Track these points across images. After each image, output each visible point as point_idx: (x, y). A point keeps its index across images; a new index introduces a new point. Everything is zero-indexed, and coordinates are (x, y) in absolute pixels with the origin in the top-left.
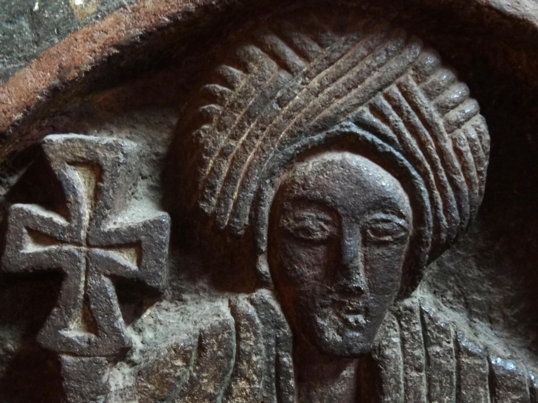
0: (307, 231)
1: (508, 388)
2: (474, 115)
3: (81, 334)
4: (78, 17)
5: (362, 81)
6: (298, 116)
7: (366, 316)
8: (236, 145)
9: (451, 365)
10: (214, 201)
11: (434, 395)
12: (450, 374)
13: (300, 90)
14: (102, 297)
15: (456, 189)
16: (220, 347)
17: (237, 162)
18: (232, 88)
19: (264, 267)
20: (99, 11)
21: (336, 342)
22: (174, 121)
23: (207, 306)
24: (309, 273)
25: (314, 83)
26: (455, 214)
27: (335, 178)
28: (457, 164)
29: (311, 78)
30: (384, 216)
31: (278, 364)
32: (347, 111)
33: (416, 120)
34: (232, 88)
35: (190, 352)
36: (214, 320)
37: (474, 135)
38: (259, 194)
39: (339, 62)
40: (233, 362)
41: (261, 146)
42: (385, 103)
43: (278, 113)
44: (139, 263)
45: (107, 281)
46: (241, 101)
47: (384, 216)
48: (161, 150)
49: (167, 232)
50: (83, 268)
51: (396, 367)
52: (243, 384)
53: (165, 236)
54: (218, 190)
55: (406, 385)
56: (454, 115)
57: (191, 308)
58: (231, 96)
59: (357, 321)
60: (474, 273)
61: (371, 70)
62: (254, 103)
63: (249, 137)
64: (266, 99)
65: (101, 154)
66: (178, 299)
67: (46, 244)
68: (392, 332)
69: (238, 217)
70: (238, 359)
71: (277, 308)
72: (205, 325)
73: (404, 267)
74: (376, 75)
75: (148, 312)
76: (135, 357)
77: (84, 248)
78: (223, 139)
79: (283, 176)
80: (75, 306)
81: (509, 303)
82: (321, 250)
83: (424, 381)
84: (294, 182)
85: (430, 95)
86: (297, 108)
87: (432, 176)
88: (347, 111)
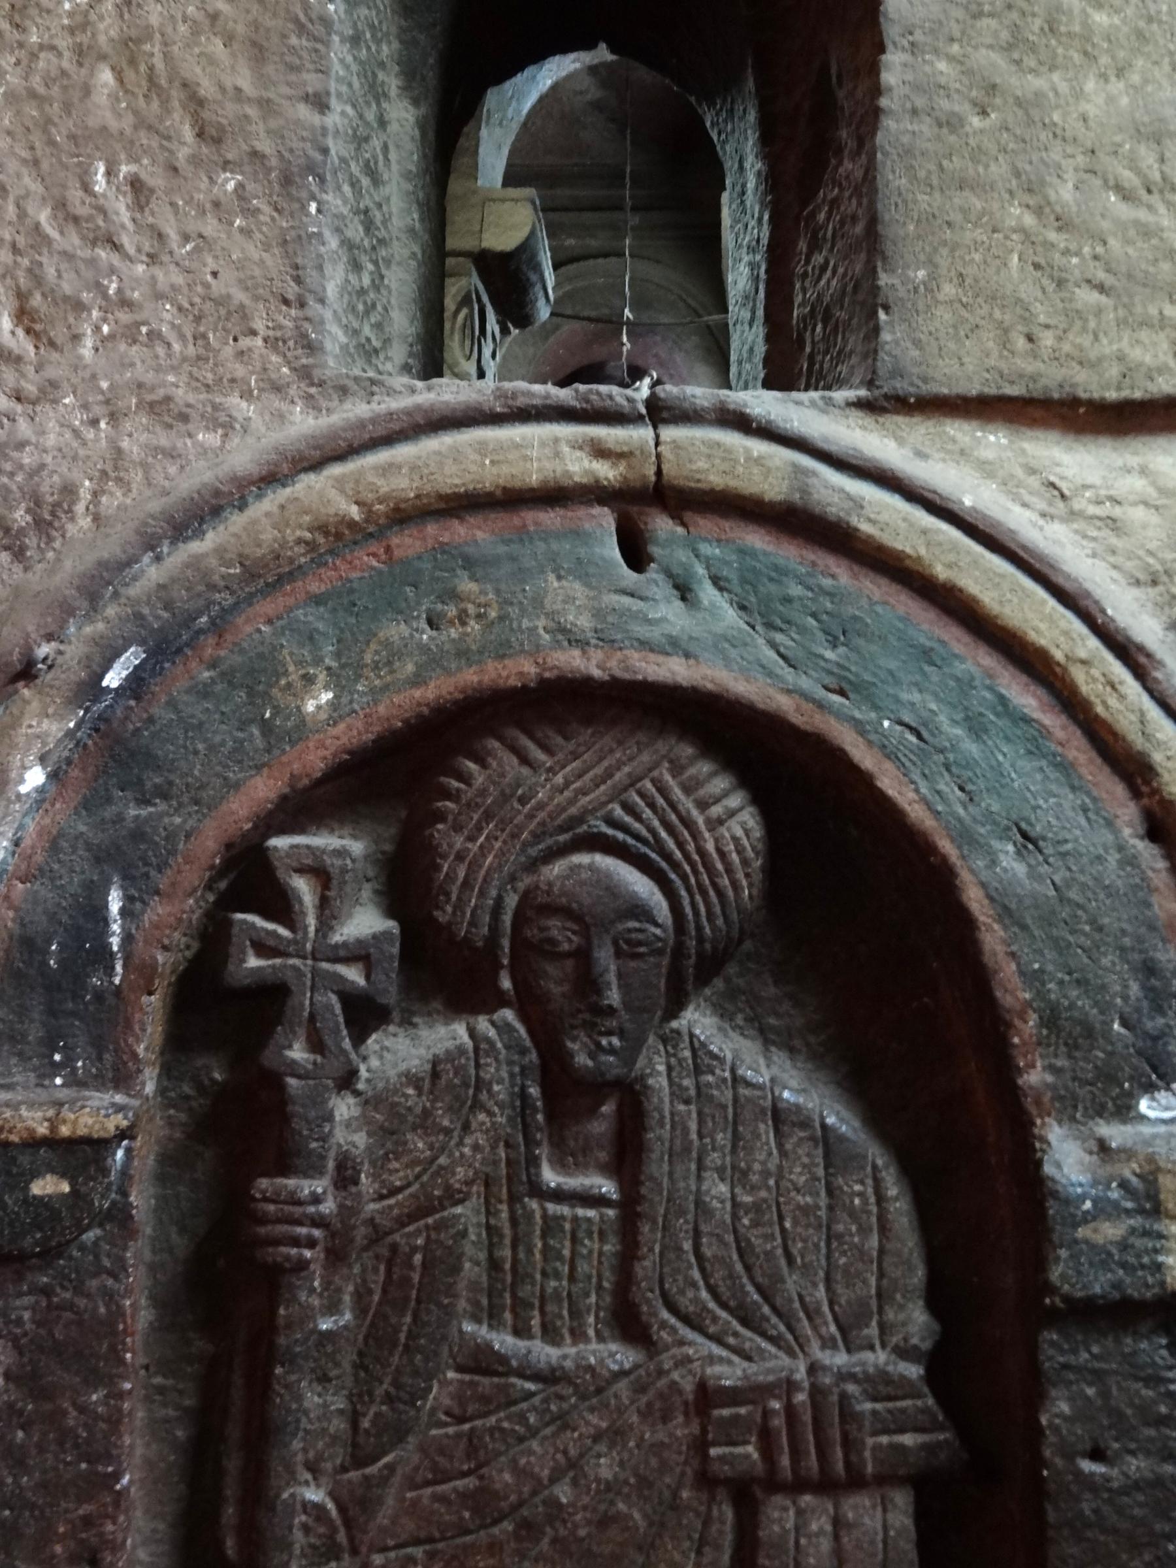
0: (552, 942)
1: (794, 1124)
2: (741, 809)
3: (306, 1056)
4: (310, 724)
5: (611, 776)
6: (542, 815)
7: (621, 1039)
8: (474, 847)
10: (449, 909)
11: (705, 1131)
12: (724, 1107)
13: (543, 787)
14: (328, 1016)
15: (720, 894)
16: (456, 1074)
18: (469, 784)
19: (506, 984)
20: (331, 717)
21: (586, 1066)
22: (403, 814)
23: (442, 1031)
24: (556, 990)
25: (559, 779)
26: (720, 922)
27: (582, 883)
28: (719, 866)
29: (555, 774)
30: (637, 925)
31: (523, 1095)
32: (595, 810)
34: (469, 784)
35: (423, 1079)
36: (450, 1044)
37: (739, 833)
38: (499, 901)
39: (585, 756)
40: (471, 1092)
41: (500, 849)
42: (638, 799)
43: (519, 812)
44: (368, 977)
45: (334, 999)
46: (478, 800)
47: (637, 925)
48: (388, 847)
49: (398, 944)
50: (309, 983)
51: (661, 1100)
52: (482, 1117)
53: (396, 950)
54: (454, 897)
55: (672, 1120)
56: (716, 810)
57: (424, 1033)
58: (469, 794)
59: (610, 1044)
60: (771, 991)
62: (493, 802)
63: (487, 838)
64: (505, 798)
66: (407, 1022)
67: (268, 957)
68: (656, 1058)
69: (476, 927)
70: (478, 1089)
71: (522, 1031)
72: (439, 1049)
73: (668, 981)
74: (627, 769)
75: (374, 1036)
76: (361, 1086)
77: (309, 962)
78: (459, 841)
79: (526, 882)
80: (300, 1024)
82: (569, 964)
83: (694, 1115)
84: (537, 887)
85: (687, 790)
86: (541, 806)
87: (693, 880)
88: (595, 810)
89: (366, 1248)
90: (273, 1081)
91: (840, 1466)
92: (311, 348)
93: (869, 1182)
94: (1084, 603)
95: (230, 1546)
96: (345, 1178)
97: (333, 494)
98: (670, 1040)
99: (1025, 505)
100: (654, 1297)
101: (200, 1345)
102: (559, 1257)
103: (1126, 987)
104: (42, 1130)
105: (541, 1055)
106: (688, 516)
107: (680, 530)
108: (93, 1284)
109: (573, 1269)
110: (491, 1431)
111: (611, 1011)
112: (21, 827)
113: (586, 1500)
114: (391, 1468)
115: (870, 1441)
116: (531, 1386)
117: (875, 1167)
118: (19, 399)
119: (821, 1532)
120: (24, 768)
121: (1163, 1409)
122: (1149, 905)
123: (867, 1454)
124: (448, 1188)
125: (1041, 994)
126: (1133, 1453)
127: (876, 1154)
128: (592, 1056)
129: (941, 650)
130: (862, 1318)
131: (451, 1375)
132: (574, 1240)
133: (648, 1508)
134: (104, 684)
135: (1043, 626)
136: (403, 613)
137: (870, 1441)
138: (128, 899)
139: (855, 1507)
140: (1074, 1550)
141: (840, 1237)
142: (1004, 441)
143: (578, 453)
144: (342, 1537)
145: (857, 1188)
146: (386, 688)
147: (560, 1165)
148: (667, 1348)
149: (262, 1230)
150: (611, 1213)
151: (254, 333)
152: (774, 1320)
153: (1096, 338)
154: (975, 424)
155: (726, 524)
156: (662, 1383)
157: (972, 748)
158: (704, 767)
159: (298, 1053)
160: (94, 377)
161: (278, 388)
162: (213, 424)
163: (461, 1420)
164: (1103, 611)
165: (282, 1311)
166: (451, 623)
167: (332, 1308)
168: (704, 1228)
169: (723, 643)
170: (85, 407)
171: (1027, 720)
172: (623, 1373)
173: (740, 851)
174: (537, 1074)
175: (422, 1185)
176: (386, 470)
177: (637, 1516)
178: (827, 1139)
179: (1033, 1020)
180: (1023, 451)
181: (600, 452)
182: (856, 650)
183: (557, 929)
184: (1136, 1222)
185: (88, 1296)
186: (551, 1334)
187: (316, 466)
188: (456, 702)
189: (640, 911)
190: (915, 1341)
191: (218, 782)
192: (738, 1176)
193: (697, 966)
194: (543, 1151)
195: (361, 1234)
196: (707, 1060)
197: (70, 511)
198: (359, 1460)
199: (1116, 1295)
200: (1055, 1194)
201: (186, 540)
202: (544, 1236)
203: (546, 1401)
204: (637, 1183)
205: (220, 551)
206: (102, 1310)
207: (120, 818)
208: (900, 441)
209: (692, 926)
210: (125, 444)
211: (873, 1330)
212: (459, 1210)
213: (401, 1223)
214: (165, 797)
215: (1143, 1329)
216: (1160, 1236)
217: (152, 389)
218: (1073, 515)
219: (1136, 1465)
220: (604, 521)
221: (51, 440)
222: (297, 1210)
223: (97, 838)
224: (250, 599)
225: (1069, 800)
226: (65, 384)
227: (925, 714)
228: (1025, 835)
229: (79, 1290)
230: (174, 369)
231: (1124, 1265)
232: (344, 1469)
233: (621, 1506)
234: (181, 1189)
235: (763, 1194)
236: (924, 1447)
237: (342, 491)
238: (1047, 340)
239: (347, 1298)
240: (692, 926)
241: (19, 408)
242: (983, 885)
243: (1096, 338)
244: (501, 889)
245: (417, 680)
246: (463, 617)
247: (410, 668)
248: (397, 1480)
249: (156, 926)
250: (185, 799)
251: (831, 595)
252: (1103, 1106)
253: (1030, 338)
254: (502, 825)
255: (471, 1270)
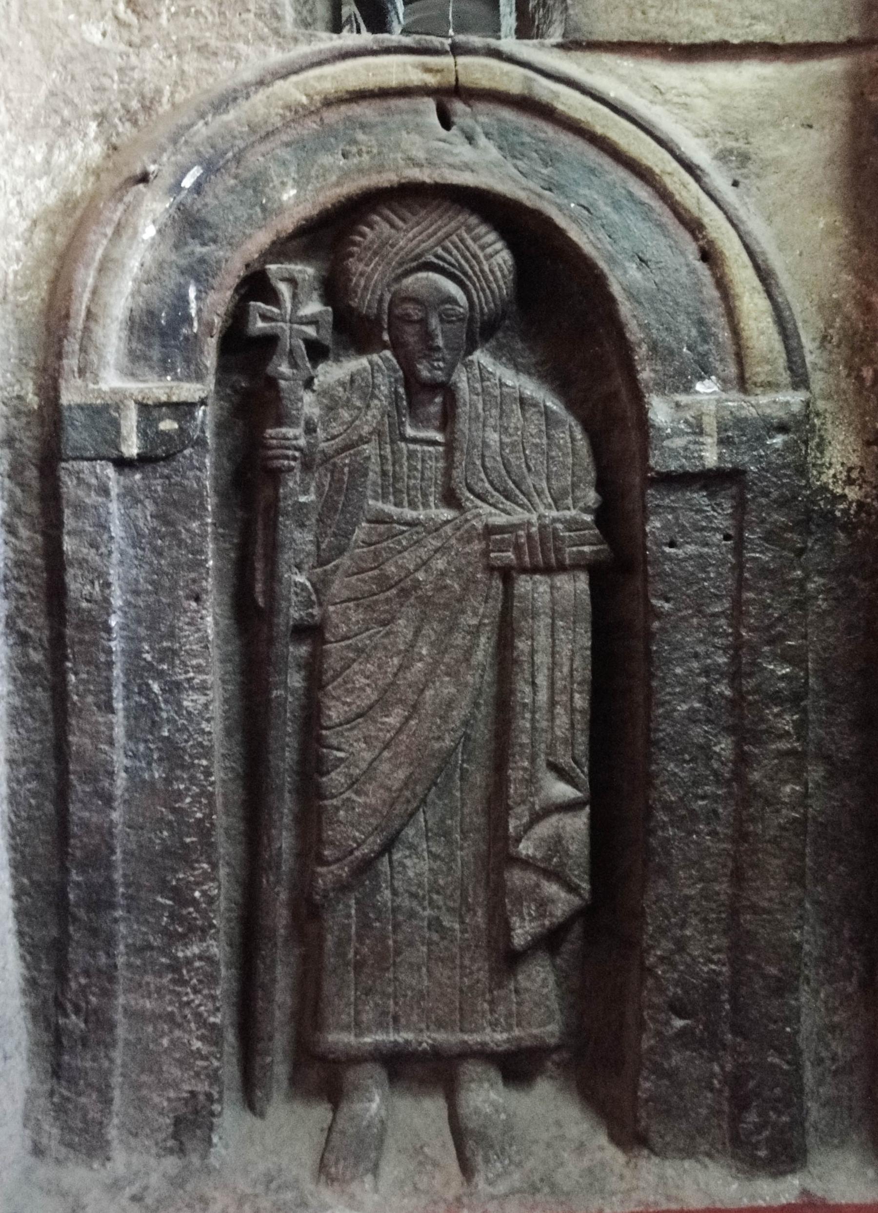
0: (408, 315)
6: (402, 253)
8: (369, 269)
9: (497, 392)
15: (492, 292)
17: (369, 279)
19: (386, 337)
24: (412, 340)
25: (410, 235)
26: (492, 305)
28: (491, 278)
31: (396, 392)
33: (468, 254)
37: (501, 262)
44: (318, 332)
45: (301, 343)
56: (489, 250)
60: (519, 346)
61: (439, 228)
65: (296, 275)
66: (337, 360)
71: (395, 361)
72: (354, 369)
76: (315, 388)
78: (361, 267)
81: (541, 363)
82: (418, 327)
85: (475, 239)
86: (402, 248)
89: (321, 465)
90: (272, 383)
91: (553, 561)
92: (279, 18)
93: (568, 433)
94: (670, 145)
95: (261, 601)
96: (310, 429)
97: (293, 90)
98: (468, 365)
99: (642, 97)
100: (462, 486)
101: (240, 514)
102: (416, 469)
103: (690, 331)
104: (164, 398)
105: (404, 373)
106: (471, 102)
107: (468, 110)
108: (190, 474)
109: (423, 473)
110: (384, 549)
111: (438, 349)
112: (144, 257)
113: (431, 578)
114: (337, 567)
115: (568, 550)
116: (404, 528)
117: (570, 426)
118: (130, 45)
119: (545, 592)
120: (145, 226)
121: (704, 524)
122: (701, 292)
123: (567, 556)
124: (361, 436)
125: (648, 335)
126: (688, 543)
127: (571, 420)
128: (430, 371)
129: (599, 169)
130: (564, 493)
131: (364, 524)
132: (423, 461)
133: (461, 582)
134: (183, 185)
135: (650, 156)
136: (329, 150)
137: (568, 550)
138: (199, 291)
139: (561, 581)
140: (661, 587)
141: (553, 458)
142: (632, 65)
143: (416, 70)
144: (314, 597)
145: (562, 435)
146: (322, 188)
147: (415, 426)
148: (469, 510)
149: (270, 453)
150: (441, 449)
151: (249, 11)
152: (521, 496)
153: (677, 12)
154: (617, 56)
155: (491, 106)
156: (467, 526)
157: (615, 217)
158: (482, 229)
159: (284, 368)
160: (168, 34)
161: (262, 39)
162: (231, 57)
163: (370, 545)
164: (679, 149)
165: (281, 491)
166: (354, 155)
167: (306, 492)
168: (487, 453)
169: (491, 166)
170: (165, 49)
171: (643, 204)
172: (447, 522)
173: (501, 271)
174: (402, 382)
175: (348, 435)
176: (320, 78)
177: (456, 586)
178: (547, 413)
179: (644, 347)
180: (641, 71)
181: (428, 70)
182: (556, 168)
183: (411, 309)
184: (691, 438)
185: (188, 479)
186: (413, 505)
187: (285, 77)
188: (357, 195)
189: (452, 300)
190: (590, 504)
191: (241, 234)
192: (504, 430)
193: (481, 328)
194: (406, 420)
195: (318, 457)
196: (487, 375)
197: (160, 101)
198: (321, 563)
199: (681, 470)
200: (653, 426)
201: (220, 114)
202: (408, 459)
203: (411, 535)
204: (453, 433)
205: (238, 120)
206: (195, 485)
207: (192, 253)
208: (579, 65)
209: (478, 307)
210: (186, 67)
211: (570, 501)
212: (365, 446)
213: (338, 452)
214: (215, 241)
215: (695, 487)
216: (703, 444)
217: (199, 40)
218: (666, 102)
219: (691, 549)
220: (429, 105)
221: (148, 66)
222: (287, 443)
223: (183, 262)
224: (253, 145)
225: (663, 241)
226: (154, 38)
227: (591, 200)
228: (641, 260)
229: (184, 476)
230: (208, 29)
231: (685, 457)
232: (314, 567)
233: (448, 582)
234: (228, 440)
235: (515, 438)
236: (593, 551)
237: (298, 89)
238: (652, 13)
239: (312, 489)
240: (478, 307)
241: (131, 50)
242: (621, 284)
243: (677, 12)
244: (382, 290)
245: (338, 184)
246: (360, 153)
247: (334, 178)
248: (339, 573)
249: (212, 304)
250: (224, 243)
251: (544, 141)
252: (678, 387)
253: (644, 13)
254: (383, 258)
255: (373, 476)
